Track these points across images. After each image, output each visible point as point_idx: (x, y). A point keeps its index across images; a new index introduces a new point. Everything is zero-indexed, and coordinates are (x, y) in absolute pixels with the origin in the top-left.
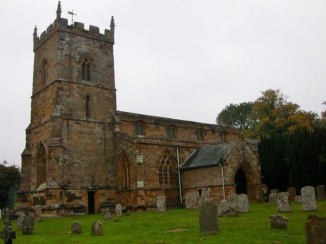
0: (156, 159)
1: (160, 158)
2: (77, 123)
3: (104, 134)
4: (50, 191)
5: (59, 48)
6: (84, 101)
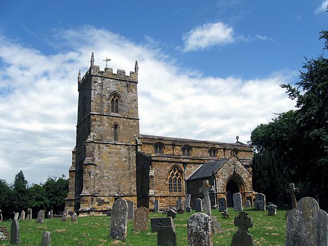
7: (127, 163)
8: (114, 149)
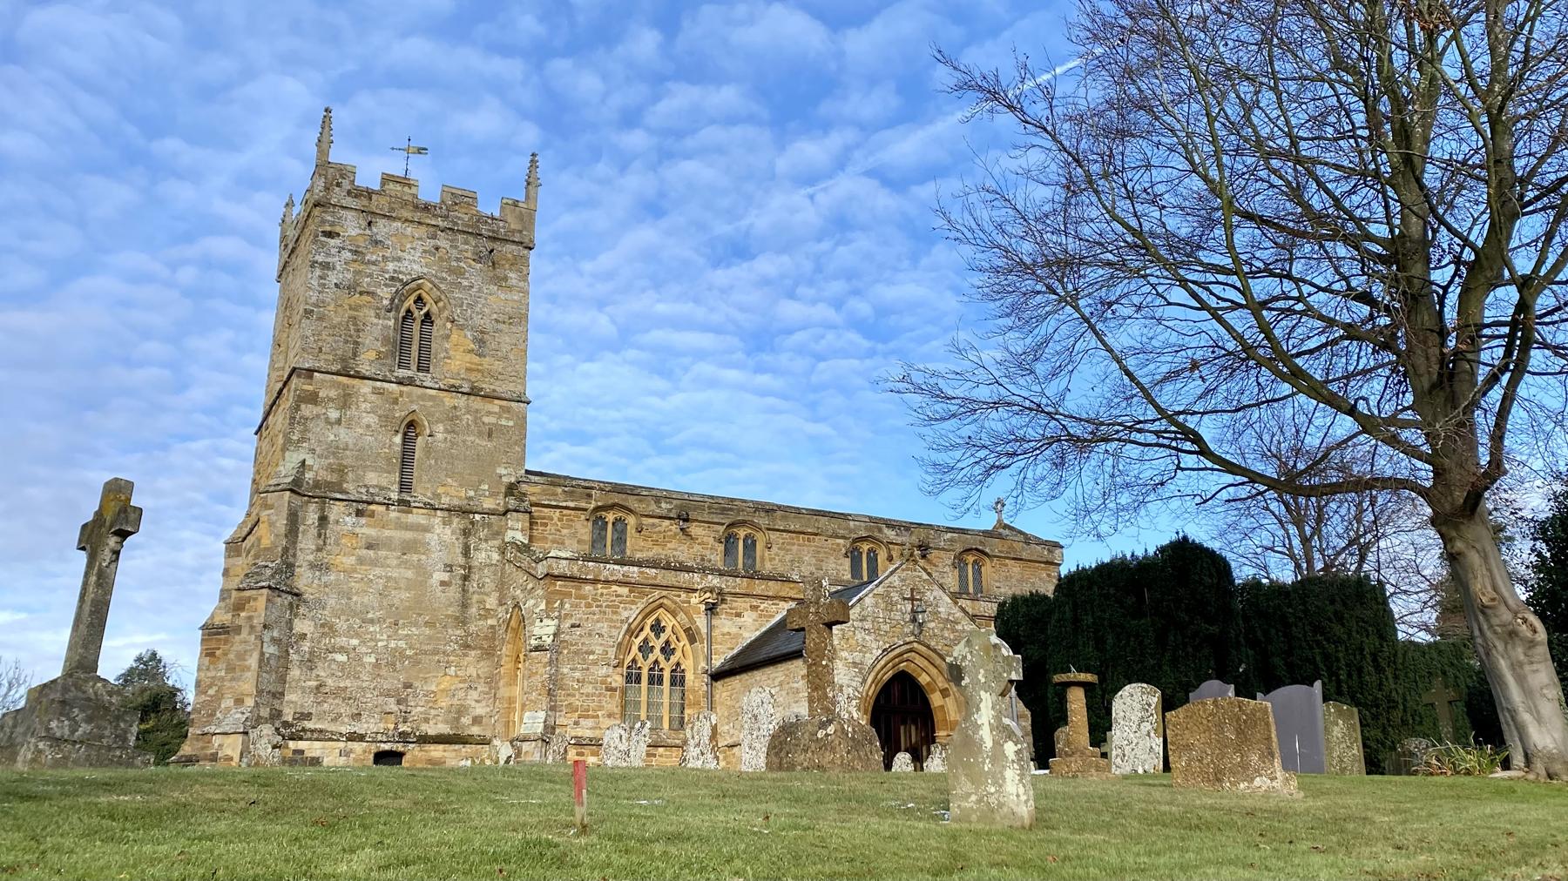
0: (614, 632)
1: (632, 633)
2: (359, 513)
3: (466, 552)
4: (217, 740)
5: (313, 264)
6: (398, 439)
7: (454, 592)
8: (389, 526)
